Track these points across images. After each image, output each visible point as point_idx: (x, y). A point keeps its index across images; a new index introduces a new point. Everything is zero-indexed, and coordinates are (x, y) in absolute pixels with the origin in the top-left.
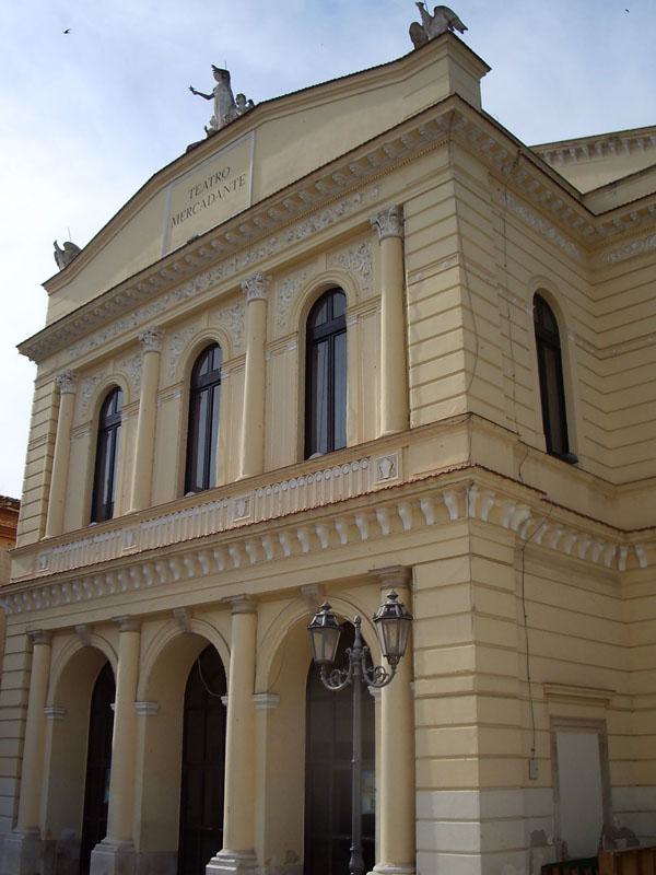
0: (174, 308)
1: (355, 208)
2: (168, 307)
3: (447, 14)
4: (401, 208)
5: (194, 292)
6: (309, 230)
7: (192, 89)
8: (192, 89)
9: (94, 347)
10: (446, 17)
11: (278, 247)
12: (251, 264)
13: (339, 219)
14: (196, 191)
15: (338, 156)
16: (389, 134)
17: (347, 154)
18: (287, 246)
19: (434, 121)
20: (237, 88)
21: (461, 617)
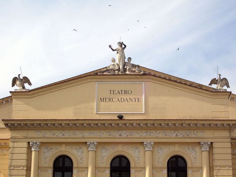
0: (105, 138)
1: (193, 136)
2: (103, 136)
3: (226, 81)
4: (212, 143)
5: (118, 136)
6: (175, 135)
7: (110, 46)
8: (110, 46)
9: (63, 136)
10: (225, 82)
11: (160, 135)
12: (147, 136)
13: (187, 136)
14: (112, 92)
15: (33, 119)
16: (206, 121)
17: (99, 120)
18: (164, 136)
19: (230, 124)
20: (128, 53)
21: (216, 159)
